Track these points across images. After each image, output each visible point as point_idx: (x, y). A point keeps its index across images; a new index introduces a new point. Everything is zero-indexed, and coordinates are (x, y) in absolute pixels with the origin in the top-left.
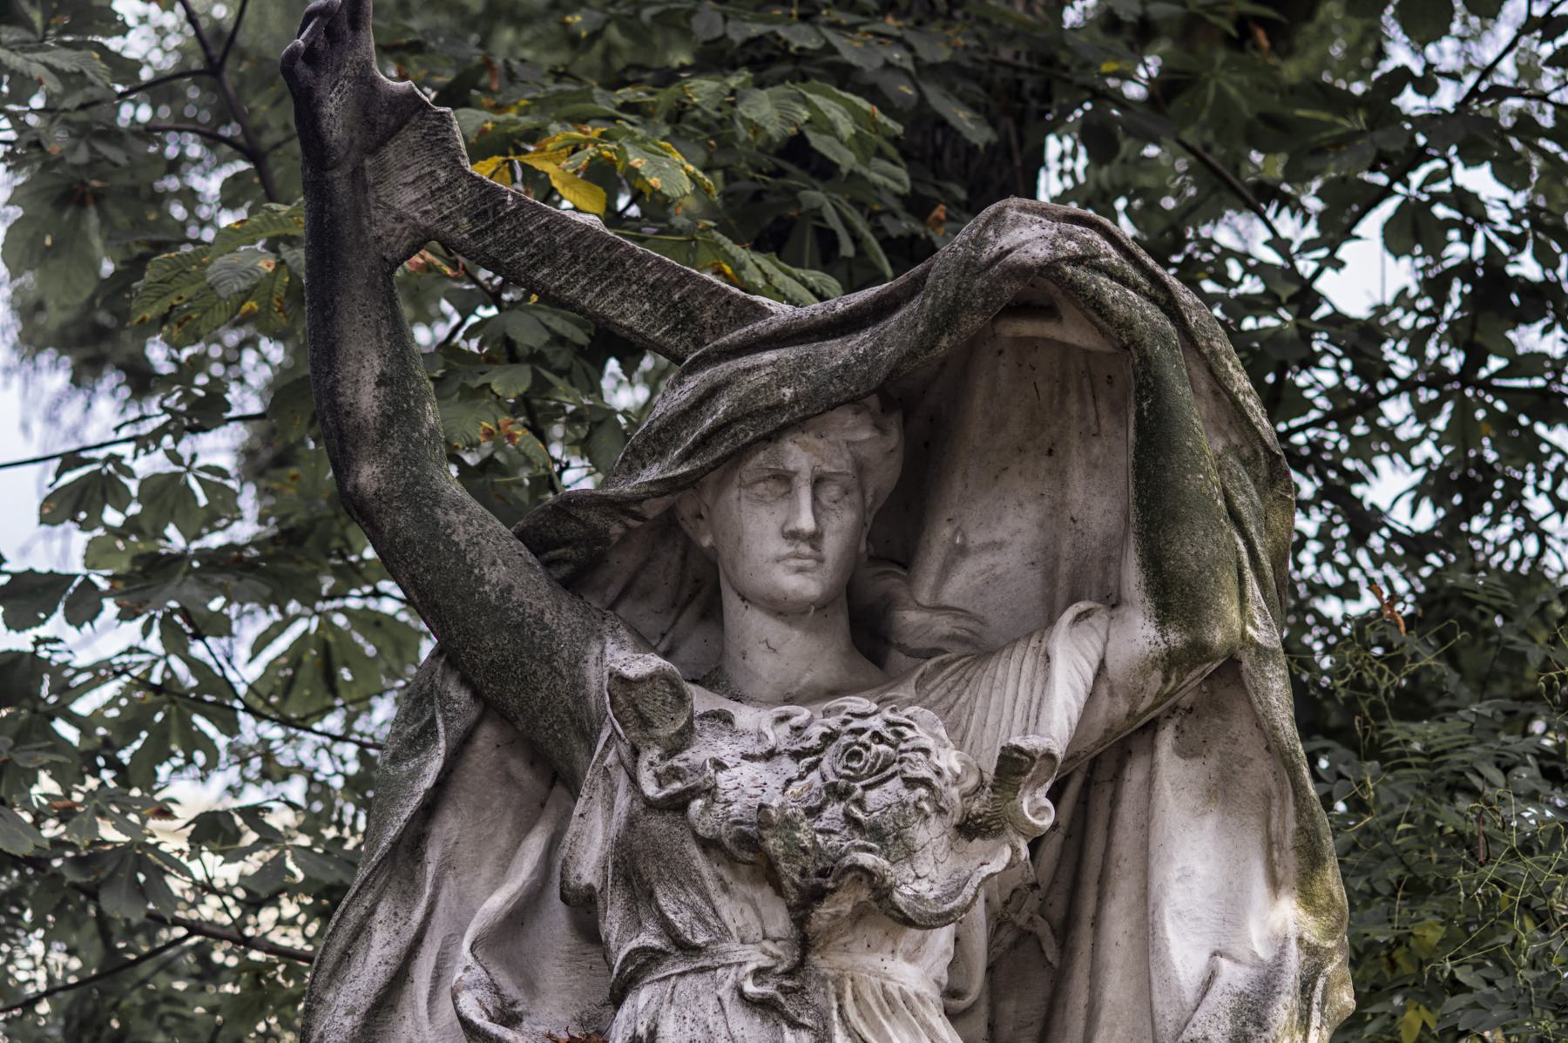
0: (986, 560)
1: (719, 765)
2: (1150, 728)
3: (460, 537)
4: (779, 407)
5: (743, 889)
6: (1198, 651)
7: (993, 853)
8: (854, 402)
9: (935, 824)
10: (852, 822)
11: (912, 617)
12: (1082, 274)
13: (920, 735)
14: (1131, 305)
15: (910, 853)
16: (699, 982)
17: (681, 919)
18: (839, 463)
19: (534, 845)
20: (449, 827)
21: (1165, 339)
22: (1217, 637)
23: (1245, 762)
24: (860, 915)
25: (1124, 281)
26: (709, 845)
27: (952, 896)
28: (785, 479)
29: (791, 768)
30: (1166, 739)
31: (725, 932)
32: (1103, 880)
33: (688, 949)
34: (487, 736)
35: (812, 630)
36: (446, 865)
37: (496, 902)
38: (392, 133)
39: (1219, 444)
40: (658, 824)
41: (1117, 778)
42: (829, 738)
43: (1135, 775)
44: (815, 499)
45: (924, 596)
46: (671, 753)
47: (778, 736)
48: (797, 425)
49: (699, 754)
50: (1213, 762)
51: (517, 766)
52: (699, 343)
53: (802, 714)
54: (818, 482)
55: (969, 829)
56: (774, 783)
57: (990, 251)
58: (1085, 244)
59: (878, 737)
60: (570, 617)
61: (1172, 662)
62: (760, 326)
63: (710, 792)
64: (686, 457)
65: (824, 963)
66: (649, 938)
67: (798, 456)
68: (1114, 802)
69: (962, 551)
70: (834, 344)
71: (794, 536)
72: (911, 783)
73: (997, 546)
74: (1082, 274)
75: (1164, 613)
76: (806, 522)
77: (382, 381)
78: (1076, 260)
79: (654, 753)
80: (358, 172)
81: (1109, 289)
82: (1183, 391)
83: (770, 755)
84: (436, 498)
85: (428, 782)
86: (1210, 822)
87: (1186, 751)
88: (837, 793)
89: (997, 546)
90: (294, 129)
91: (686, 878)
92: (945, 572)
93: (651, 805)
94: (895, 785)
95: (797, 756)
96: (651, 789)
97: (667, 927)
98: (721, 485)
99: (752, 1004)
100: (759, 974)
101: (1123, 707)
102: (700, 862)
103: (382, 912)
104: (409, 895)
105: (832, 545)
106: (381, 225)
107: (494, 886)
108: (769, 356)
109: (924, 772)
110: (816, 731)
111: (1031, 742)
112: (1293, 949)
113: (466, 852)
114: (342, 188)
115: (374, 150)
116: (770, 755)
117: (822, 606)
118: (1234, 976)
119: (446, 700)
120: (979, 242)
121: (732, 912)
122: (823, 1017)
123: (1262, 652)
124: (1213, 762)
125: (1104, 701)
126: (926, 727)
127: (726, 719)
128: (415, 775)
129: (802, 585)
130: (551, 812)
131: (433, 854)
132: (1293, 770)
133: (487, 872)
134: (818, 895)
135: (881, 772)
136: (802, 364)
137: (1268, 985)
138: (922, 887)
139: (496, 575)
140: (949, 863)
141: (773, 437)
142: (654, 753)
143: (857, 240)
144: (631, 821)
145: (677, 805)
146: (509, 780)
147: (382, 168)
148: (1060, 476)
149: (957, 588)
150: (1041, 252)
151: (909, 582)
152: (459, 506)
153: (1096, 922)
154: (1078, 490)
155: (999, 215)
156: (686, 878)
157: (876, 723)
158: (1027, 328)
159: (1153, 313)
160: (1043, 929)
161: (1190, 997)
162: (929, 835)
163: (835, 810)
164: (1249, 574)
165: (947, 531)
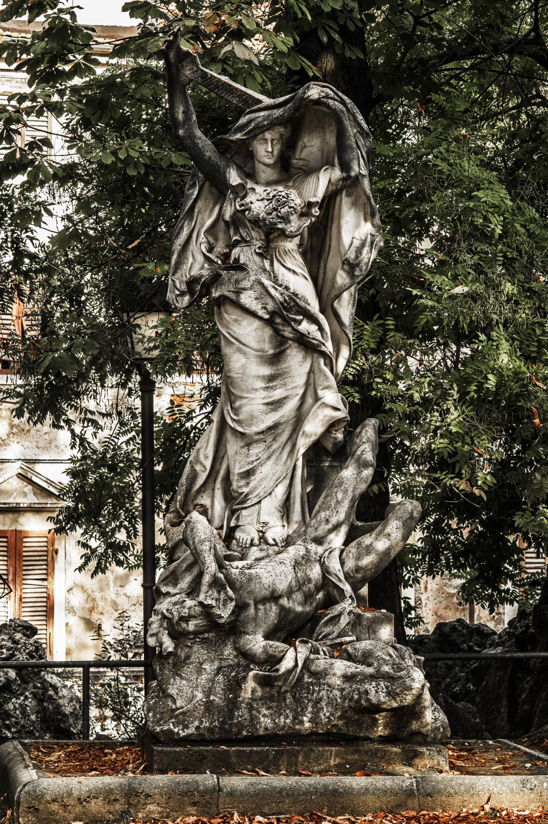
0: (310, 149)
1: (252, 203)
2: (341, 190)
3: (200, 146)
4: (264, 126)
5: (256, 229)
6: (349, 177)
7: (307, 220)
8: (280, 125)
9: (295, 215)
10: (277, 215)
11: (294, 161)
12: (325, 100)
13: (292, 196)
14: (335, 105)
15: (289, 222)
16: (248, 248)
17: (244, 235)
18: (277, 136)
19: (217, 209)
20: (200, 204)
21: (343, 112)
22: (353, 174)
23: (360, 197)
24: (279, 236)
25: (335, 100)
26: (250, 221)
27: (298, 230)
28: (266, 140)
29: (266, 203)
30: (344, 193)
31: (253, 238)
32: (332, 220)
33: (246, 242)
34: (207, 185)
35: (273, 168)
36: (199, 212)
37: (209, 223)
38: (184, 59)
39: (355, 131)
40: (240, 215)
41: (335, 199)
42: (274, 196)
43: (338, 199)
44: (272, 143)
45: (297, 157)
46: (241, 200)
47: (264, 195)
48: (268, 129)
49: (248, 200)
50: (353, 197)
51: (214, 190)
52: (249, 108)
53: (269, 189)
54: (272, 140)
55: (302, 215)
56: (263, 206)
57: (306, 96)
58: (326, 93)
59: (284, 197)
60: (223, 163)
61: (343, 179)
62: (260, 106)
63: (250, 209)
64: (245, 135)
65: (272, 245)
66: (237, 238)
67: (268, 135)
68: (335, 203)
69: (305, 147)
70: (275, 111)
71: (268, 152)
72: (290, 207)
73: (312, 146)
74: (325, 100)
75: (342, 170)
76: (270, 149)
77: (183, 112)
78: (324, 97)
79: (239, 200)
80: (178, 66)
81: (331, 102)
82: (347, 123)
83: (262, 200)
84: (195, 137)
85: (194, 196)
86: (352, 211)
87: (347, 196)
88: (275, 209)
89: (312, 146)
90: (156, 393)
91: (245, 226)
92: (301, 151)
93: (238, 211)
94: (287, 207)
95: (268, 200)
96: (238, 207)
97: (241, 236)
98: (253, 140)
99: (258, 254)
100: (259, 248)
101: (334, 188)
102: (248, 223)
103: (186, 224)
104: (191, 220)
105: (276, 153)
106: (183, 78)
107: (210, 216)
108: (262, 114)
109: (292, 205)
110: (271, 195)
111: (313, 200)
112: (369, 237)
113: (203, 209)
114: (174, 71)
115: (181, 62)
116: (262, 200)
117: (275, 164)
118: (357, 243)
119: (198, 177)
120: (304, 93)
121: (254, 234)
122: (272, 256)
123: (363, 176)
124: (353, 197)
125: (331, 187)
126: (293, 194)
127: (253, 189)
128: (192, 194)
129: (270, 161)
130: (220, 202)
131: (196, 210)
132: (369, 200)
133: (207, 213)
134: (271, 233)
135: (284, 204)
136: (269, 116)
137: (363, 245)
138: (292, 229)
139: (208, 154)
140: (298, 223)
141: (263, 132)
142: (239, 200)
143: (303, 13)
144: (234, 213)
145: (243, 211)
146: (212, 193)
147: (183, 66)
148: (324, 133)
149: (304, 154)
150: (316, 96)
151: (294, 153)
152: (200, 138)
153: (331, 228)
154: (328, 137)
155: (309, 86)
156: (245, 226)
157: (283, 194)
158: (316, 107)
159: (341, 106)
160: (321, 227)
161: (347, 248)
162: (294, 218)
163: (275, 213)
164: (361, 159)
165: (301, 143)
